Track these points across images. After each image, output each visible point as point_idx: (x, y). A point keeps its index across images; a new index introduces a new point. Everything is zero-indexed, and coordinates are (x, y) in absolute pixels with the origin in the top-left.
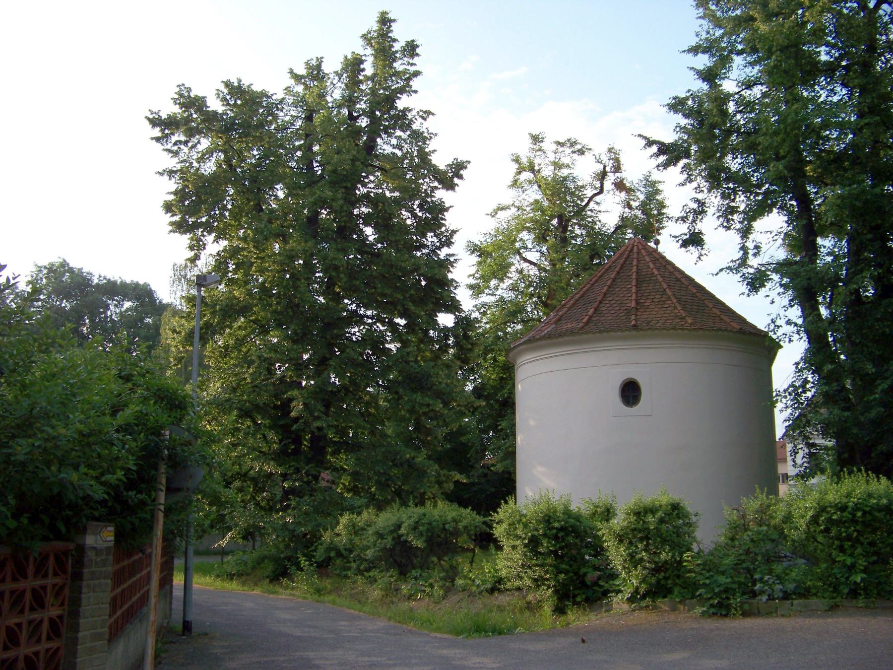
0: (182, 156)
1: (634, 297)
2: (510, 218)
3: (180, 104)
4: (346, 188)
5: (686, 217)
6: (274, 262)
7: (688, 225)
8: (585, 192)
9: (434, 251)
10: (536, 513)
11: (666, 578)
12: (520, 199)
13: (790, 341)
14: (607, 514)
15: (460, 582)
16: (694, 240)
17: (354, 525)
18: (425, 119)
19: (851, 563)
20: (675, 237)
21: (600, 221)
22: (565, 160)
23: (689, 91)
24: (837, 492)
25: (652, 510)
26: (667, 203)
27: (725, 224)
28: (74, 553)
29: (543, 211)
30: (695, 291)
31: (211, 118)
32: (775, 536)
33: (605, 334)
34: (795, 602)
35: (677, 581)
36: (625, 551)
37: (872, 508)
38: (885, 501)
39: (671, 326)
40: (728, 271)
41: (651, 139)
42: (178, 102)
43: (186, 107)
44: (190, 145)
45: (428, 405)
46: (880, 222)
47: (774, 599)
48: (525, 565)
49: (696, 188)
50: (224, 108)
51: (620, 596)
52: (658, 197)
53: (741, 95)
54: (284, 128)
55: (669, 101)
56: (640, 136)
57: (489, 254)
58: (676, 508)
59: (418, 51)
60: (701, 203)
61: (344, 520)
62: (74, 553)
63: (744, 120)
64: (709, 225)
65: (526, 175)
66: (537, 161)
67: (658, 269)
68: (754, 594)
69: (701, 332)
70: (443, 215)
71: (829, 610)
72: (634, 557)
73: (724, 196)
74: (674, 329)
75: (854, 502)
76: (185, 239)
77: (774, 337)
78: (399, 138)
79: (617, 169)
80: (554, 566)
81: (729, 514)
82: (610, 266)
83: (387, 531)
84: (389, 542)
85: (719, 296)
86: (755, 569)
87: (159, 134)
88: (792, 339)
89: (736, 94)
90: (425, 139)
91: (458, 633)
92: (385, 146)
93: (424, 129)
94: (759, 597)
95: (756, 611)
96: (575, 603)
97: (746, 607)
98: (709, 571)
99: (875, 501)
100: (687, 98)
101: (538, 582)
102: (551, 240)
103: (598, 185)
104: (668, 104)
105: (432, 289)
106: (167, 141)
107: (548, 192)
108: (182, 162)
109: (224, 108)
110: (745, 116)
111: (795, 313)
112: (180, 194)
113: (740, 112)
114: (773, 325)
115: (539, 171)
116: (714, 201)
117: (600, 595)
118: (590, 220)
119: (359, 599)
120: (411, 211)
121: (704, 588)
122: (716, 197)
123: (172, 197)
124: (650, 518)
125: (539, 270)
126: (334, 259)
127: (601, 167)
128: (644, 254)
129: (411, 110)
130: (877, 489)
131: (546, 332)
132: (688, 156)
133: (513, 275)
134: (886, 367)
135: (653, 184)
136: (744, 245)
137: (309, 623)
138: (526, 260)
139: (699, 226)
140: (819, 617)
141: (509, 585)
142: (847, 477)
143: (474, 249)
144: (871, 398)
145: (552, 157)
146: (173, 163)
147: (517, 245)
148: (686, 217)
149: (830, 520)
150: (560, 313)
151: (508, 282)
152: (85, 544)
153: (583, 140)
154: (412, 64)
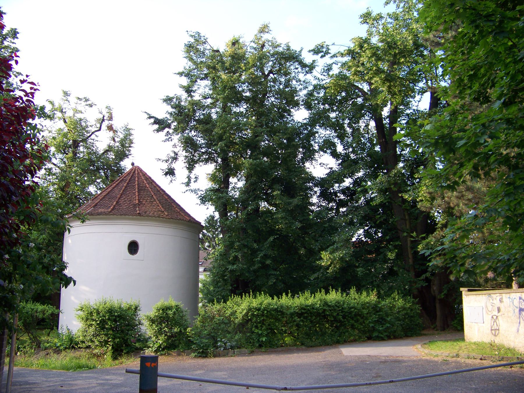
1: (137, 198)
5: (168, 160)
7: (168, 164)
16: (171, 172)
20: (163, 170)
22: (79, 108)
23: (175, 95)
25: (169, 308)
30: (167, 198)
32: (226, 321)
33: (123, 216)
34: (235, 350)
39: (157, 216)
41: (151, 115)
51: (150, 349)
52: (131, 138)
59: (18, 35)
66: (64, 107)
67: (149, 184)
69: (171, 220)
79: (111, 118)
80: (113, 335)
82: (123, 179)
91: (68, 369)
94: (220, 349)
95: (218, 355)
100: (173, 98)
103: (99, 126)
107: (437, 262)
115: (65, 112)
116: (182, 154)
124: (170, 312)
127: (102, 116)
128: (141, 175)
131: (89, 211)
136: (189, 176)
139: (174, 165)
140: (247, 356)
145: (73, 106)
148: (168, 160)
149: (253, 315)
154: (13, 43)
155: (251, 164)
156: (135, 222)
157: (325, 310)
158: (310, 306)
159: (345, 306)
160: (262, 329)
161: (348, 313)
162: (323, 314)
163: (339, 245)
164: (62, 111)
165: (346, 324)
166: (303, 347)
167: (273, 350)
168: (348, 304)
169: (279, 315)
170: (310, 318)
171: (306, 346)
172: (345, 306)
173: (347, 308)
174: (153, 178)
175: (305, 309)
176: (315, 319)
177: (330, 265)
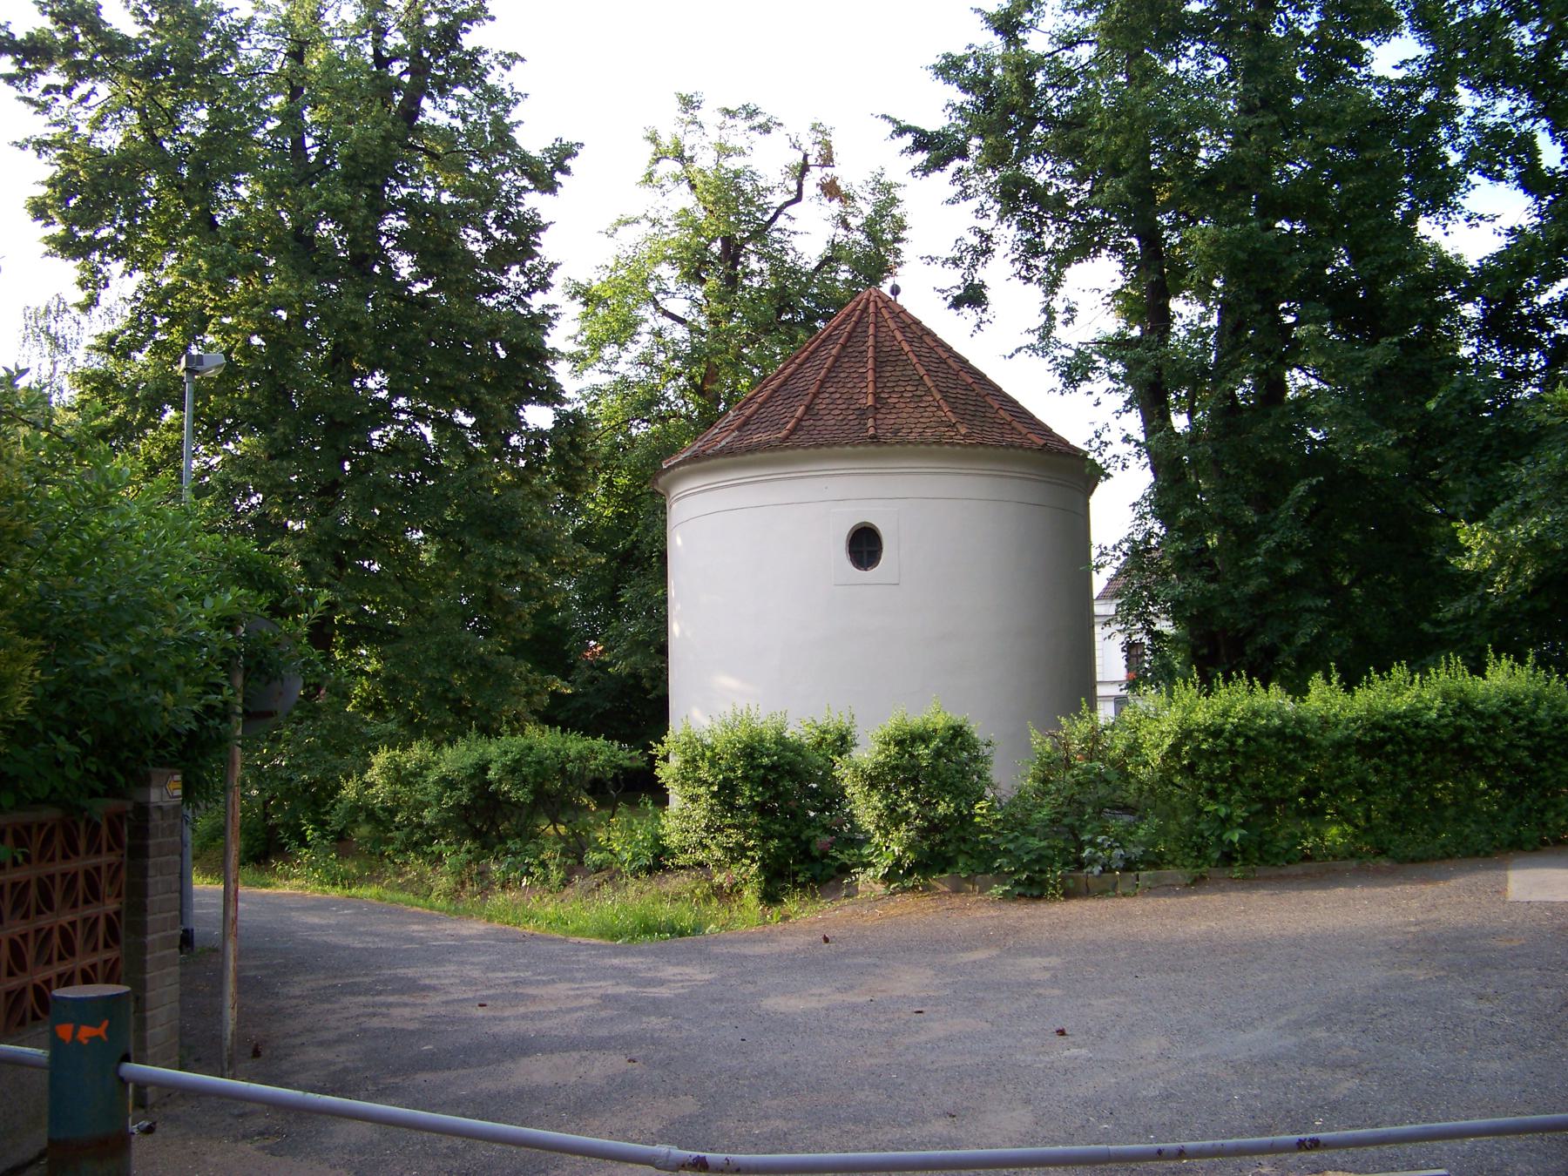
0: (56, 112)
2: (639, 240)
3: (52, 14)
4: (372, 187)
5: (960, 258)
6: (247, 317)
7: (961, 271)
8: (770, 198)
9: (520, 301)
10: (730, 742)
11: (943, 842)
12: (658, 206)
13: (1124, 466)
14: (843, 742)
15: (594, 857)
16: (972, 296)
17: (397, 769)
18: (508, 68)
19: (1227, 815)
20: (943, 291)
21: (793, 249)
23: (970, 47)
24: (1208, 707)
25: (923, 737)
26: (908, 221)
27: (1023, 273)
28: (131, 816)
29: (698, 231)
31: (116, 46)
33: (824, 449)
34: (1143, 874)
35: (962, 847)
36: (880, 801)
37: (1260, 733)
38: (1277, 722)
39: (932, 439)
40: (1030, 352)
42: (48, 9)
43: (66, 22)
44: (76, 94)
45: (515, 564)
46: (1272, 284)
47: (1112, 871)
48: (712, 827)
49: (977, 211)
50: (140, 29)
51: (870, 871)
52: (896, 211)
53: (1055, 60)
54: (248, 73)
55: (936, 61)
56: (885, 117)
57: (602, 301)
58: (957, 735)
60: (986, 238)
61: (381, 759)
62: (131, 816)
63: (1058, 99)
64: (998, 273)
65: (670, 166)
66: (687, 142)
68: (1080, 865)
69: (981, 449)
70: (537, 237)
71: (1192, 884)
72: (894, 810)
73: (1022, 225)
74: (938, 443)
75: (1232, 724)
76: (69, 270)
77: (1099, 460)
78: (460, 99)
79: (827, 160)
80: (761, 827)
81: (1041, 743)
82: (830, 335)
83: (462, 775)
84: (464, 795)
85: (1008, 389)
86: (1082, 827)
87: (14, 70)
88: (1127, 463)
89: (1049, 55)
90: (508, 104)
92: (434, 113)
93: (504, 85)
94: (1089, 869)
96: (796, 884)
97: (1070, 883)
98: (1012, 830)
99: (1264, 722)
101: (737, 853)
102: (713, 282)
103: (793, 186)
104: (935, 66)
105: (519, 366)
106: (28, 84)
108: (56, 124)
109: (140, 29)
110: (1060, 93)
111: (1133, 423)
112: (63, 186)
113: (1053, 86)
114: (1098, 441)
115: (691, 159)
116: (1007, 235)
117: (833, 871)
118: (777, 246)
119: (421, 888)
120: (484, 229)
121: (1004, 856)
122: (1009, 226)
123: (45, 190)
124: (921, 750)
125: (691, 331)
126: (352, 311)
127: (800, 159)
129: (486, 52)
130: (1265, 705)
131: (723, 443)
132: (963, 155)
133: (645, 339)
134: (1272, 515)
135: (887, 188)
136: (1048, 305)
137: (362, 929)
138: (666, 313)
139: (981, 274)
140: (1178, 894)
141: (682, 860)
142: (1221, 685)
143: (587, 296)
144: (1251, 562)
145: (714, 135)
146: (39, 127)
147: (652, 287)
148: (960, 258)
149: (1197, 751)
150: (747, 412)
151: (634, 350)
152: (148, 802)
153: (769, 108)
155: (1215, 241)
156: (872, 465)
157: (1461, 730)
158: (1405, 715)
159: (1541, 713)
160: (1229, 799)
161: (1550, 737)
162: (1455, 745)
163: (1532, 496)
164: (680, 157)
165: (1545, 779)
166: (1384, 862)
167: (1273, 871)
168: (1551, 708)
169: (1290, 751)
170: (1405, 757)
171: (1393, 857)
172: (1541, 713)
173: (1550, 720)
174: (927, 323)
175: (1384, 729)
176: (1424, 762)
177: (1495, 570)
